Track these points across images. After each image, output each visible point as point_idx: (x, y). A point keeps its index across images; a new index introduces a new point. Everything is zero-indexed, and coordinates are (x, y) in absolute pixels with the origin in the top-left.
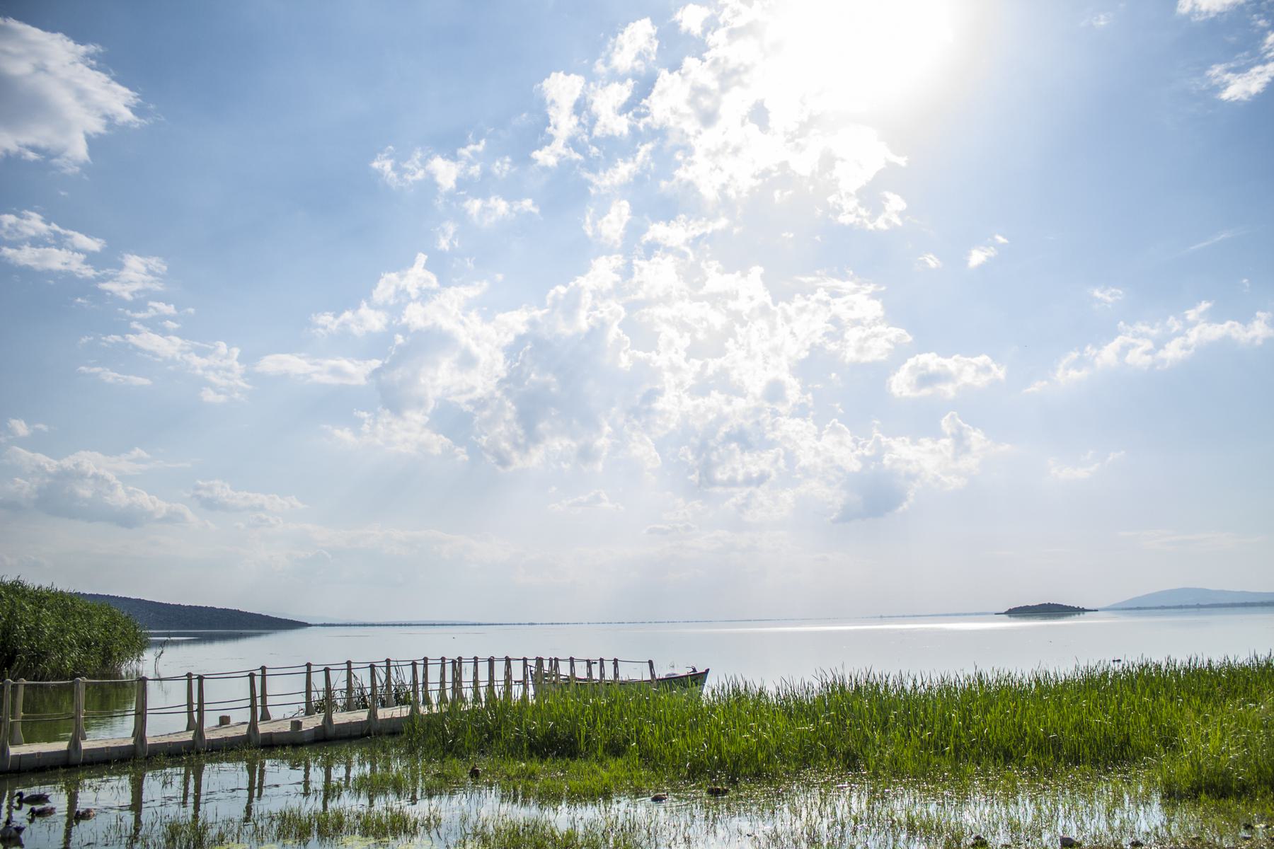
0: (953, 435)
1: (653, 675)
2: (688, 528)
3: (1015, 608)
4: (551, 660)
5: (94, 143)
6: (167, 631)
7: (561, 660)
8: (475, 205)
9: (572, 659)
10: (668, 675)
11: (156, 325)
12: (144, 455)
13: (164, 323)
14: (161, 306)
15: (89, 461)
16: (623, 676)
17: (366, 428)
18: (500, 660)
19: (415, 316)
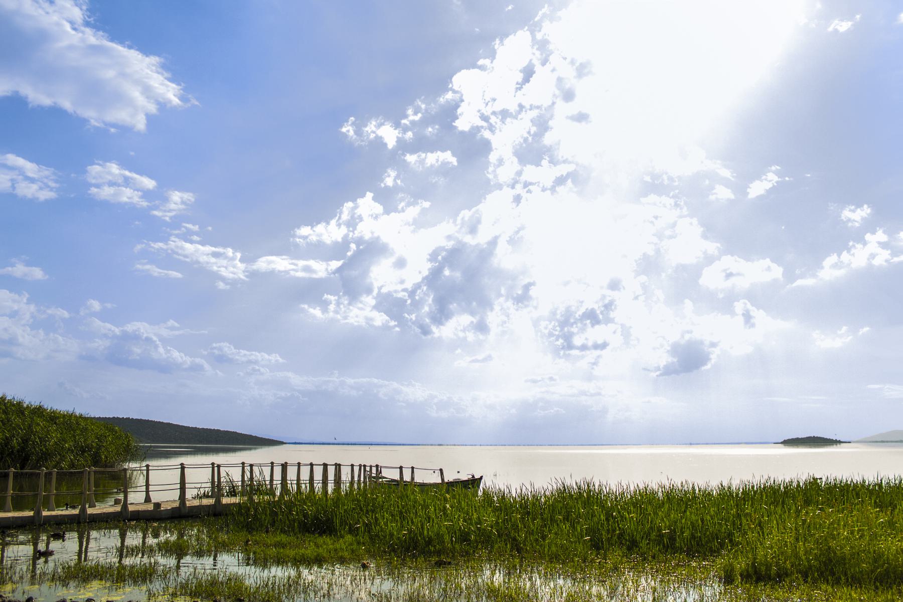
0: (743, 314)
1: (443, 479)
2: (551, 379)
3: (789, 440)
4: (360, 466)
5: (149, 118)
6: (234, 446)
7: (316, 465)
8: (411, 158)
9: (299, 464)
10: (455, 479)
11: (187, 237)
12: (176, 325)
13: (192, 237)
14: (190, 226)
15: (143, 328)
16: (418, 480)
17: (332, 307)
18: (292, 465)
19: (365, 230)
